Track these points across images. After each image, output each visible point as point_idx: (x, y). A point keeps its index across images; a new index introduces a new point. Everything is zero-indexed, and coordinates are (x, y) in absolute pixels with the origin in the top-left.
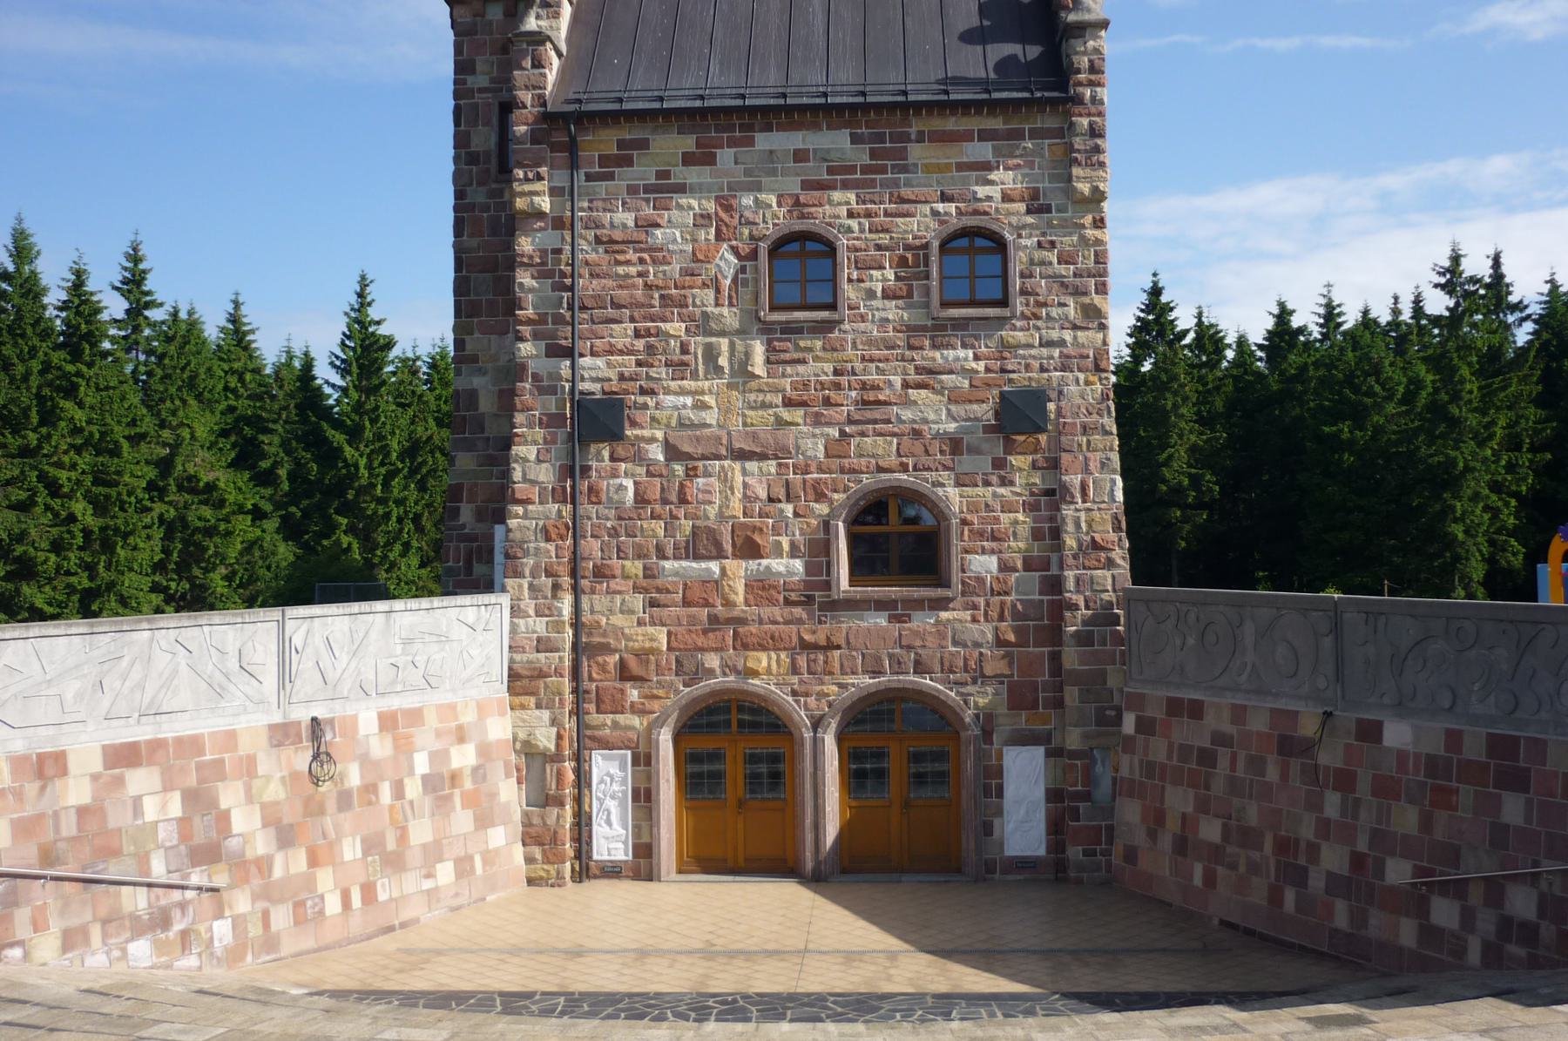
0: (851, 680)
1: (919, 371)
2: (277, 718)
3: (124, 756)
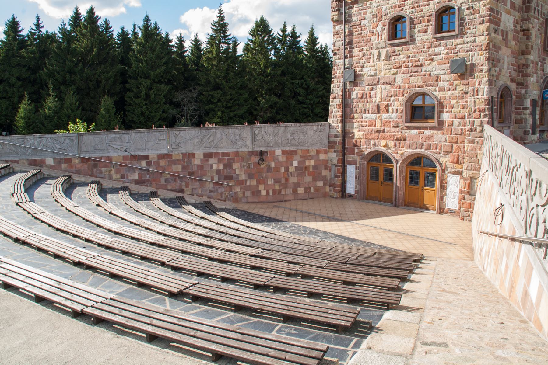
0: (408, 150)
1: (429, 55)
2: (250, 150)
3: (208, 156)
